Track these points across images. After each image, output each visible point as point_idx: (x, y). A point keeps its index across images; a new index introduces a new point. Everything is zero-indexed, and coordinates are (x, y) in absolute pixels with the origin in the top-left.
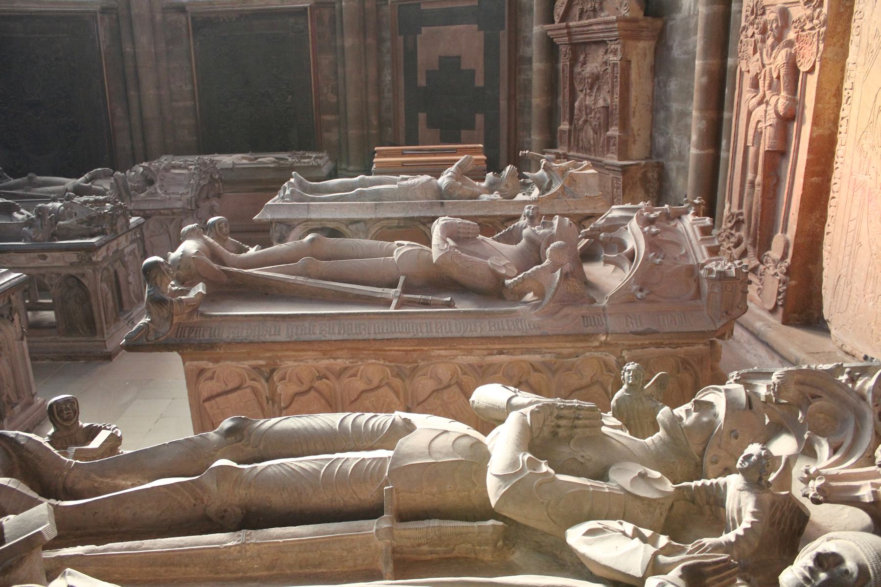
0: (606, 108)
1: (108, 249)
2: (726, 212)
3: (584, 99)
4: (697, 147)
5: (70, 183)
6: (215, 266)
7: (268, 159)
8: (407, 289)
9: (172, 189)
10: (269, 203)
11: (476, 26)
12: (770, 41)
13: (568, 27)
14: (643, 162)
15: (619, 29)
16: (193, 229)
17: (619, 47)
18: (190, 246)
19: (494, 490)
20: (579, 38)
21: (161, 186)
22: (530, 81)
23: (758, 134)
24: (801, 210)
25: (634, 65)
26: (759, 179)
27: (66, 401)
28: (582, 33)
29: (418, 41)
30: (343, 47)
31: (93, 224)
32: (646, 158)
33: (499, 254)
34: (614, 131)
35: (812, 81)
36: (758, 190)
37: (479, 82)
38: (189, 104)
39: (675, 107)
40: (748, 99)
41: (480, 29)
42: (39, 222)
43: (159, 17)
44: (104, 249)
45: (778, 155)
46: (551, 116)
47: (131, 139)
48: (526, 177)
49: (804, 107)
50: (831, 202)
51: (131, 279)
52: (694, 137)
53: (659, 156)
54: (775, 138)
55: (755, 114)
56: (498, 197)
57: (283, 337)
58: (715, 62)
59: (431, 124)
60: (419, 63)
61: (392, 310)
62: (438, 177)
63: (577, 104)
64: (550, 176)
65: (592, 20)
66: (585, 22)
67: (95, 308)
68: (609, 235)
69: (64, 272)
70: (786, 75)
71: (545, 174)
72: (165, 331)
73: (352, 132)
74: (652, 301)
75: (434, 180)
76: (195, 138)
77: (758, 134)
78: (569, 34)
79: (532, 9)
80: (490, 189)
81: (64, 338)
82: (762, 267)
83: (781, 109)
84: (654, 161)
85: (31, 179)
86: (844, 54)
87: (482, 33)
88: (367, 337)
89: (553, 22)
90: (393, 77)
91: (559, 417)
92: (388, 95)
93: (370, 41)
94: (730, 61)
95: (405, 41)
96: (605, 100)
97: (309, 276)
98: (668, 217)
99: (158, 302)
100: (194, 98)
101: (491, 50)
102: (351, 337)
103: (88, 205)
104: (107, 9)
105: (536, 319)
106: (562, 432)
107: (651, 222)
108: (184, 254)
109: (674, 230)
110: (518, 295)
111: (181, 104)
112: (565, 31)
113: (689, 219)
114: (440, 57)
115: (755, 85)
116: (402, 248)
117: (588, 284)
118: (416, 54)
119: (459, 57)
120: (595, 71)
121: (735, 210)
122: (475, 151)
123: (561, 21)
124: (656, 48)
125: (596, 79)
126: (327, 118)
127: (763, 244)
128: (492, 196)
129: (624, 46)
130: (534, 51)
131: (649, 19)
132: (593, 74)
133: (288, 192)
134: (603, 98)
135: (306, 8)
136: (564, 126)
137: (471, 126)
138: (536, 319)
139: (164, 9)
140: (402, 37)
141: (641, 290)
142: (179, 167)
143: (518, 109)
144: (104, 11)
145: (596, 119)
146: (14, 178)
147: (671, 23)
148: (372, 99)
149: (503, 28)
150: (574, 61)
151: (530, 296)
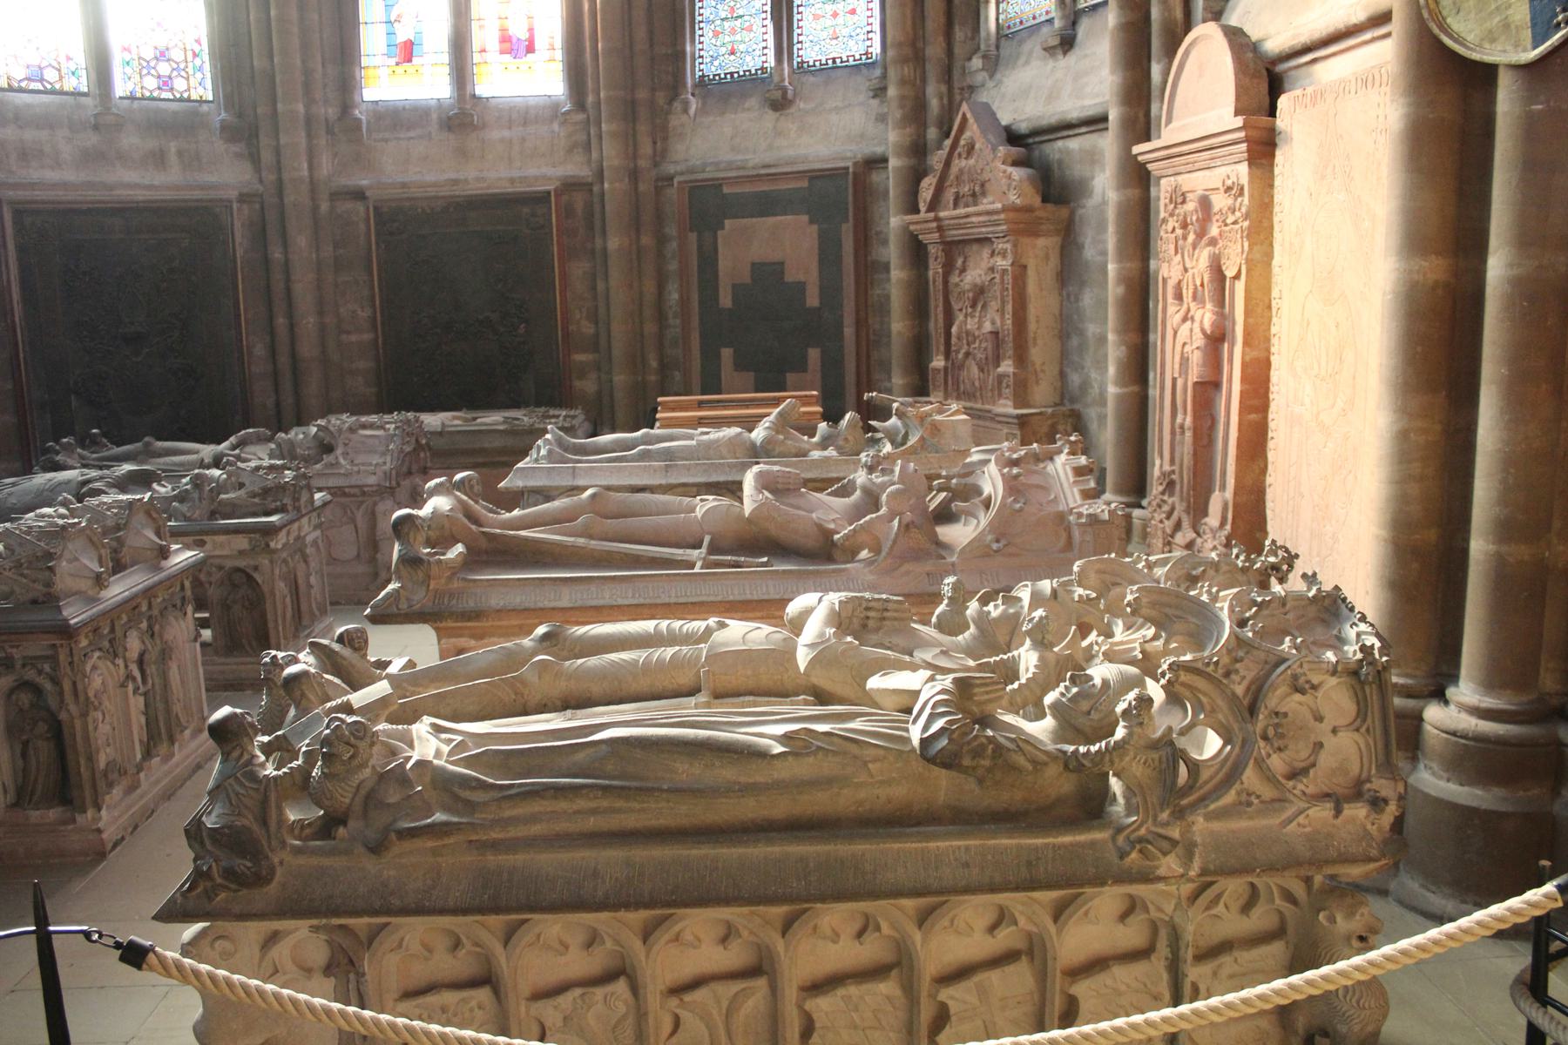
0: (995, 334)
1: (288, 534)
2: (1156, 472)
3: (965, 322)
4: (1116, 384)
5: (207, 451)
6: (473, 527)
7: (493, 419)
8: (714, 549)
9: (360, 459)
10: (520, 465)
11: (805, 218)
12: (1191, 237)
13: (937, 219)
14: (1050, 410)
15: (1007, 221)
16: (441, 484)
17: (1008, 246)
18: (439, 503)
19: (803, 658)
20: (955, 234)
21: (345, 454)
22: (888, 297)
23: (1184, 361)
24: (1239, 458)
25: (1031, 272)
26: (1189, 421)
27: (357, 630)
28: (960, 227)
29: (720, 240)
30: (605, 249)
31: (270, 496)
32: (1056, 405)
33: (829, 510)
34: (1007, 367)
35: (1240, 287)
36: (1188, 434)
37: (813, 300)
38: (367, 337)
39: (1092, 329)
40: (1174, 314)
41: (811, 222)
42: (196, 495)
43: (324, 207)
44: (284, 532)
45: (1209, 388)
46: (919, 350)
47: (277, 391)
48: (875, 430)
49: (1234, 323)
50: (1271, 444)
51: (313, 580)
52: (1112, 370)
53: (1073, 400)
54: (1204, 365)
55: (1181, 335)
56: (834, 453)
57: (565, 603)
58: (1134, 265)
59: (739, 366)
60: (721, 274)
61: (697, 570)
62: (750, 431)
63: (954, 330)
64: (906, 425)
65: (971, 210)
66: (961, 211)
67: (270, 617)
68: (963, 481)
69: (229, 564)
70: (1211, 281)
71: (899, 423)
72: (420, 598)
73: (620, 379)
74: (1010, 555)
75: (746, 434)
76: (373, 390)
77: (1184, 361)
78: (940, 229)
79: (887, 192)
80: (823, 445)
81: (222, 660)
82: (1199, 541)
83: (1207, 326)
84: (1068, 406)
85: (148, 444)
86: (1269, 255)
87: (815, 227)
88: (667, 600)
89: (917, 211)
91: (867, 609)
92: (674, 321)
93: (647, 240)
94: (1153, 264)
95: (699, 240)
96: (993, 323)
97: (591, 537)
98: (1037, 458)
99: (411, 562)
100: (374, 327)
102: (648, 601)
103: (261, 472)
104: (248, 195)
105: (871, 577)
106: (871, 623)
107: (1015, 463)
108: (435, 513)
109: (1043, 473)
110: (852, 554)
111: (353, 338)
112: (934, 225)
113: (1061, 459)
114: (753, 264)
115: (1179, 297)
116: (705, 505)
117: (939, 544)
118: (717, 260)
120: (978, 281)
121: (1167, 468)
122: (806, 401)
123: (929, 210)
124: (1063, 248)
125: (980, 292)
126: (580, 357)
127: (1198, 510)
128: (826, 453)
129: (1015, 246)
130: (892, 252)
131: (1049, 206)
132: (976, 285)
133: (543, 452)
134: (992, 319)
135: (549, 193)
136: (938, 362)
137: (801, 366)
138: (871, 577)
139: (331, 194)
141: (998, 541)
142: (371, 426)
143: (871, 340)
144: (243, 198)
145: (981, 349)
146: (118, 445)
147: (1081, 212)
148: (650, 328)
149: (847, 221)
150: (948, 267)
151: (864, 554)
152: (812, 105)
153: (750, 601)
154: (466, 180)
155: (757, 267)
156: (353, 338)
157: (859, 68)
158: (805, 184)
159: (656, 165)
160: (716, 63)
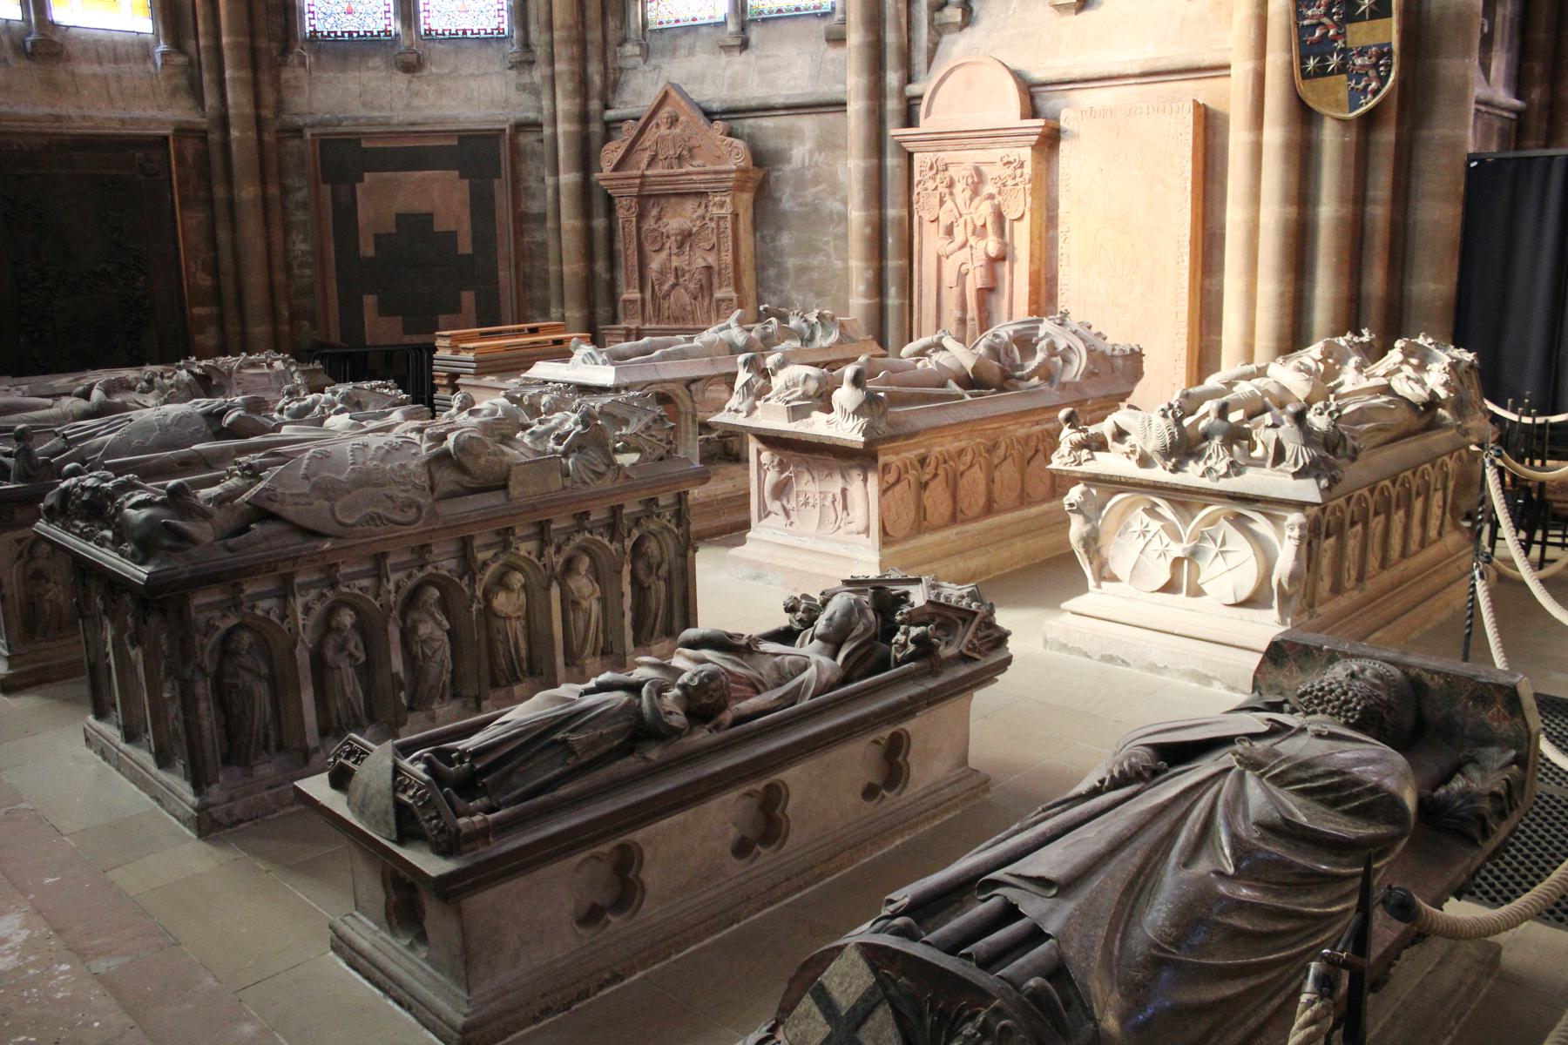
11: (457, 173)
15: (736, 180)
29: (359, 193)
37: (465, 247)
41: (462, 176)
57: (951, 421)
58: (875, 212)
60: (360, 224)
87: (466, 182)
93: (273, 190)
101: (482, 206)
114: (398, 215)
119: (431, 215)
126: (198, 311)
135: (166, 138)
137: (455, 308)
140: (329, 187)
152: (446, 70)
154: (70, 118)
155: (401, 218)
157: (486, 41)
158: (455, 142)
159: (277, 115)
160: (331, 20)
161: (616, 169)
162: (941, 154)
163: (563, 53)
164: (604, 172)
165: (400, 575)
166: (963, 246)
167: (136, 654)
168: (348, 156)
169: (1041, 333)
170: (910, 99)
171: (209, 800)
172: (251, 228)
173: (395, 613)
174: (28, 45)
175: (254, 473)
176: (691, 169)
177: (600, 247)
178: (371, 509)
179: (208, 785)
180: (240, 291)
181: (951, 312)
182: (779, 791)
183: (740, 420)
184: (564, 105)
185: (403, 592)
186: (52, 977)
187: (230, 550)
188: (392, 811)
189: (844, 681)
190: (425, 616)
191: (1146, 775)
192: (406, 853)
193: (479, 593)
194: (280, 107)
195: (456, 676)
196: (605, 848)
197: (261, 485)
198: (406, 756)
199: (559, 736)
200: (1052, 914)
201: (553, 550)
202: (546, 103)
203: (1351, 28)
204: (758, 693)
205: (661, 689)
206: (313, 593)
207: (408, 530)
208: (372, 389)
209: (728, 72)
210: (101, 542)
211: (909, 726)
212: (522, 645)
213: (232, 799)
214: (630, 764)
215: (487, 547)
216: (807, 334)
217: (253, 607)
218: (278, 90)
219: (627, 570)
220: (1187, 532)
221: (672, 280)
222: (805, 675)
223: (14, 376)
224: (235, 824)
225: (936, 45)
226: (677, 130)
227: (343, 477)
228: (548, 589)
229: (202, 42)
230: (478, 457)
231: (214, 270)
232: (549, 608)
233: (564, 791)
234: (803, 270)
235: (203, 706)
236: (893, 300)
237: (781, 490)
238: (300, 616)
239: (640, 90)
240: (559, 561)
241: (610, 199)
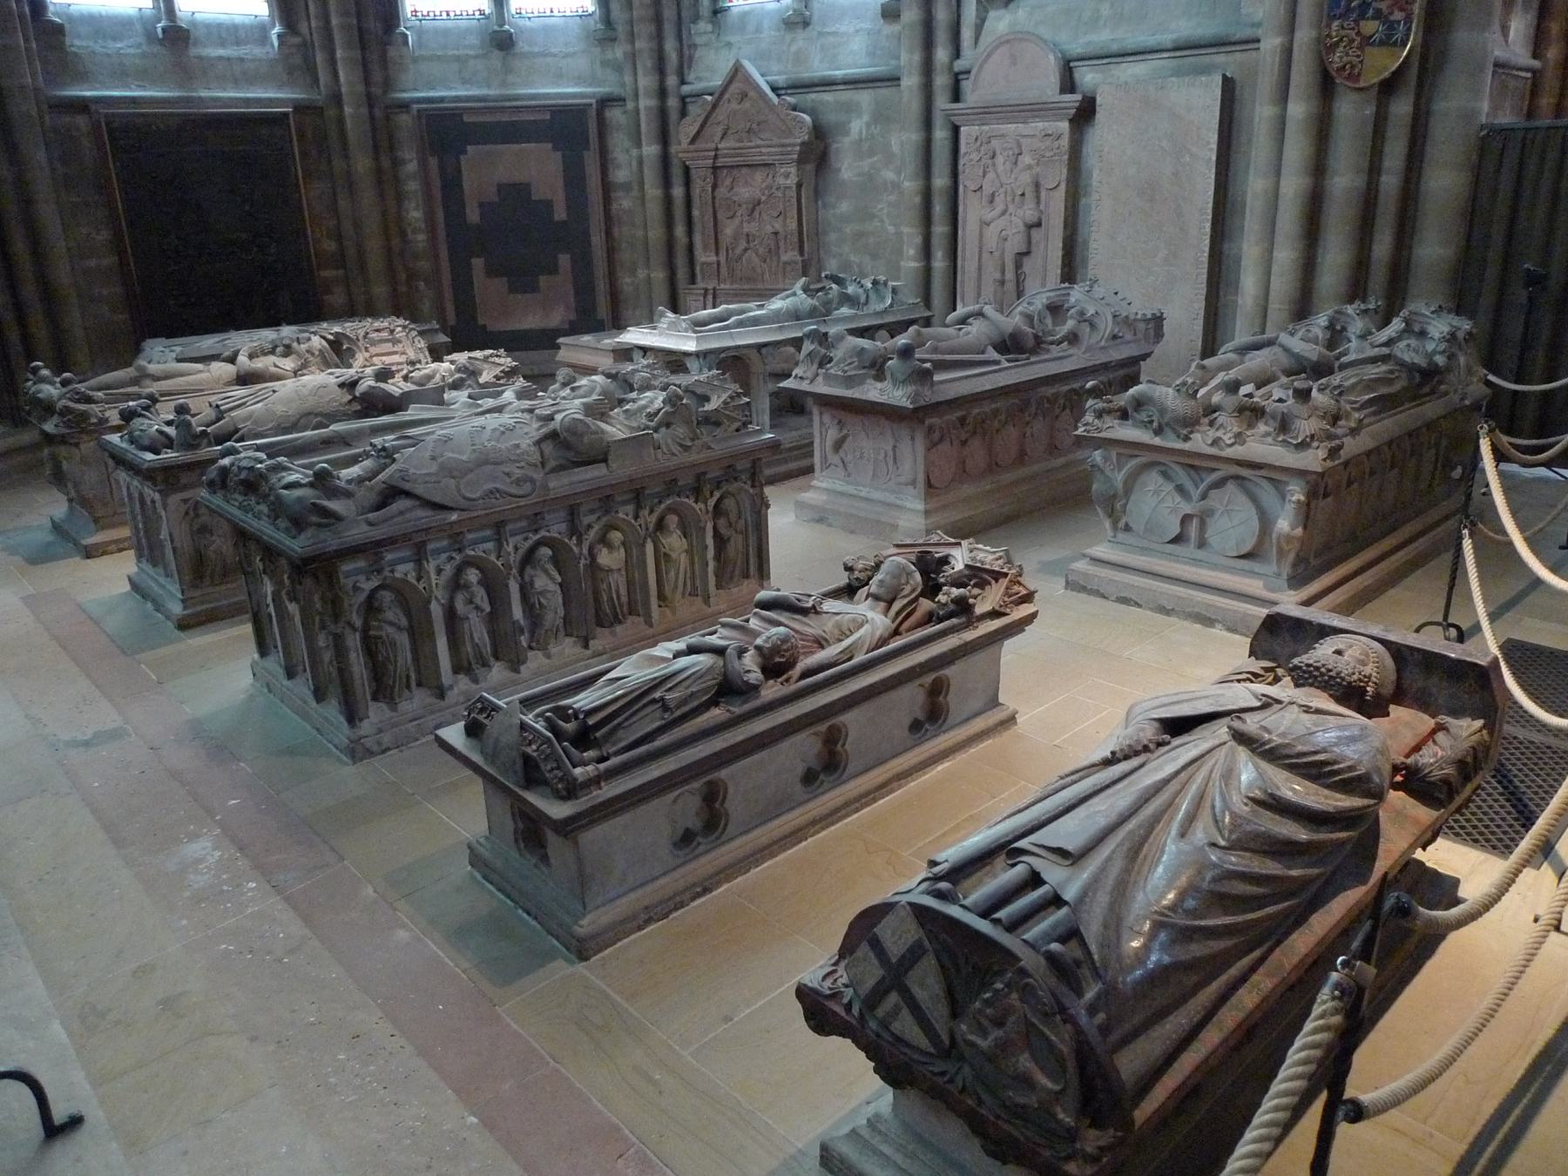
11: (550, 146)
37: (560, 214)
87: (559, 154)
90: (400, 219)
93: (386, 163)
101: (574, 180)
111: (92, 263)
119: (528, 185)
135: (286, 115)
137: (553, 270)
153: (939, 404)
156: (92, 263)
161: (693, 141)
162: (985, 128)
163: (645, 30)
164: (681, 146)
165: (519, 538)
166: (1004, 213)
167: (293, 608)
168: (449, 131)
169: (1072, 300)
170: (957, 74)
171: (362, 733)
172: (368, 196)
173: (514, 571)
174: (159, 31)
175: (387, 455)
176: (760, 142)
177: (677, 213)
178: (490, 486)
179: (361, 720)
180: (361, 253)
181: (991, 274)
182: (839, 730)
183: (805, 386)
184: (646, 81)
185: (521, 552)
186: (243, 894)
187: (370, 524)
188: (520, 762)
189: (896, 633)
190: (539, 572)
191: (1152, 746)
192: (531, 797)
193: (585, 551)
194: (388, 84)
195: (567, 620)
196: (697, 785)
197: (394, 467)
198: (531, 710)
199: (657, 695)
200: (1067, 881)
201: (646, 512)
202: (628, 79)
203: (1362, 23)
204: (823, 647)
205: (741, 652)
206: (444, 556)
207: (523, 502)
208: (486, 359)
209: (794, 48)
210: (258, 516)
211: (948, 672)
212: (623, 592)
213: (380, 731)
214: (716, 714)
215: (592, 511)
216: (863, 299)
217: (392, 571)
218: (385, 68)
219: (710, 526)
220: (1196, 494)
221: (743, 244)
222: (862, 631)
223: (168, 337)
224: (384, 752)
225: (983, 20)
226: (747, 104)
227: (464, 458)
228: (643, 545)
229: (313, 24)
230: (582, 435)
231: (339, 237)
232: (644, 562)
233: (660, 742)
234: (860, 235)
235: (353, 655)
236: (939, 262)
237: (838, 445)
238: (433, 576)
239: (710, 70)
240: (653, 519)
241: (687, 170)
